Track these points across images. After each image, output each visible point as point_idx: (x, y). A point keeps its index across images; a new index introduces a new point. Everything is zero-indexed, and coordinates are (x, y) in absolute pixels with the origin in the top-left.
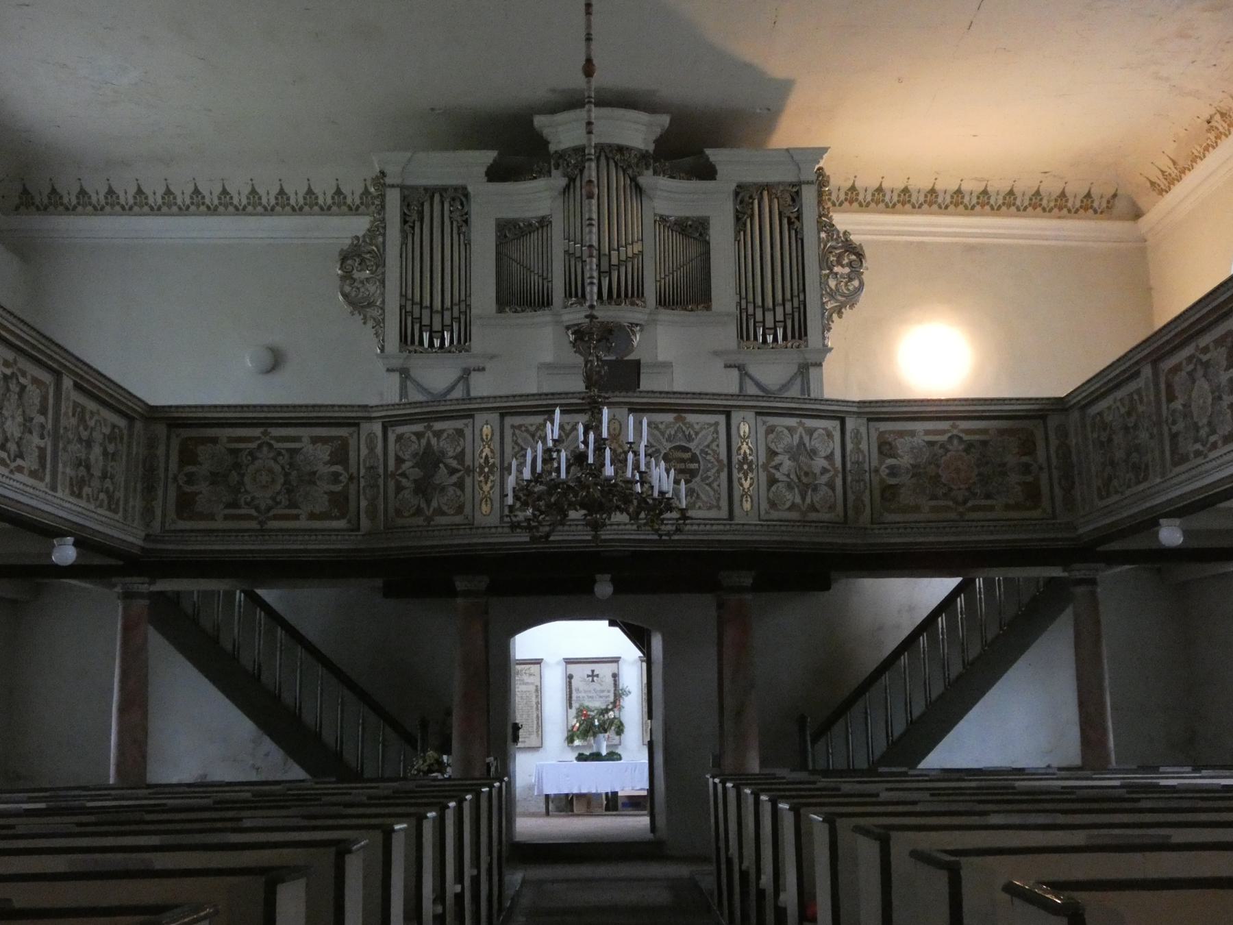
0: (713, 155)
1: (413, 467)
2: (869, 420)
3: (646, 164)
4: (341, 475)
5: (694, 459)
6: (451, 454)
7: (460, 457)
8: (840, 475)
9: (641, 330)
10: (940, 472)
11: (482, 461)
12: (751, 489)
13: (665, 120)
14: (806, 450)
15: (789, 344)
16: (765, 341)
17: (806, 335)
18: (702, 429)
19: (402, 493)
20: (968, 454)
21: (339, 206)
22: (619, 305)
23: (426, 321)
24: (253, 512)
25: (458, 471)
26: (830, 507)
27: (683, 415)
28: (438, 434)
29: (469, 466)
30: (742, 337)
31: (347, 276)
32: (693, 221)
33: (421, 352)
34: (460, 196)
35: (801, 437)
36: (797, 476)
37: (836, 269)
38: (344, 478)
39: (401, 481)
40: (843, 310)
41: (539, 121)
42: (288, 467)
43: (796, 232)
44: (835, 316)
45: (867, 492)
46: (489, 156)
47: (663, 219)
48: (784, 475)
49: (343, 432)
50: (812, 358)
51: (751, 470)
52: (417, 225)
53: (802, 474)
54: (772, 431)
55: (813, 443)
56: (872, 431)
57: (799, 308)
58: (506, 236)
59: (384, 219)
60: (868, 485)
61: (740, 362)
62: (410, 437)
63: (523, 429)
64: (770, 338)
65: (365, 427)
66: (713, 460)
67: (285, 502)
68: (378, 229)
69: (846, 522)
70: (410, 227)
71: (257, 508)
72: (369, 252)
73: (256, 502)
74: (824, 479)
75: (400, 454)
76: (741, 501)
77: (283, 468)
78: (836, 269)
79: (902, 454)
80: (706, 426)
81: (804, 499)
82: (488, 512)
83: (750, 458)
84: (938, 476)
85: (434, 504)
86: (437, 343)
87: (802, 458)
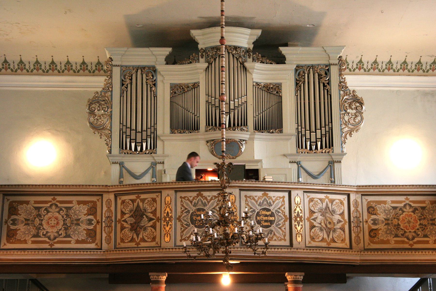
0: (284, 50)
1: (130, 217)
2: (362, 195)
3: (249, 55)
4: (93, 220)
5: (272, 215)
6: (150, 211)
7: (154, 212)
8: (347, 224)
9: (246, 143)
10: (400, 224)
11: (165, 215)
12: (301, 230)
13: (259, 32)
14: (330, 211)
15: (324, 151)
16: (311, 149)
17: (332, 146)
18: (276, 199)
19: (124, 230)
20: (414, 214)
21: (84, 71)
22: (235, 130)
23: (133, 137)
24: (47, 239)
25: (153, 219)
26: (342, 240)
27: (267, 192)
28: (143, 200)
29: (158, 217)
30: (299, 147)
31: (92, 113)
32: (273, 85)
33: (131, 154)
34: (153, 70)
35: (327, 204)
36: (325, 224)
37: (348, 111)
38: (94, 222)
39: (124, 224)
40: (352, 133)
41: (195, 33)
42: (65, 216)
43: (328, 91)
44: (348, 136)
45: (362, 232)
46: (167, 51)
47: (258, 84)
48: (319, 223)
49: (94, 199)
50: (335, 158)
51: (302, 221)
52: (129, 86)
53: (328, 222)
54: (312, 201)
55: (333, 207)
56: (364, 201)
57: (329, 131)
58: (175, 93)
59: (112, 83)
60: (362, 229)
61: (298, 160)
62: (128, 202)
63: (186, 199)
64: (314, 147)
65: (106, 197)
66: (282, 216)
67: (64, 234)
68: (109, 87)
69: (351, 247)
70: (125, 87)
71: (49, 238)
72: (104, 101)
73: (49, 234)
74: (339, 226)
75: (123, 210)
76: (296, 237)
77: (63, 217)
78: (348, 111)
79: (380, 213)
80: (278, 198)
81: (328, 236)
82: (168, 241)
83: (301, 215)
84: (399, 225)
85: (141, 236)
86: (139, 149)
87: (327, 215)
